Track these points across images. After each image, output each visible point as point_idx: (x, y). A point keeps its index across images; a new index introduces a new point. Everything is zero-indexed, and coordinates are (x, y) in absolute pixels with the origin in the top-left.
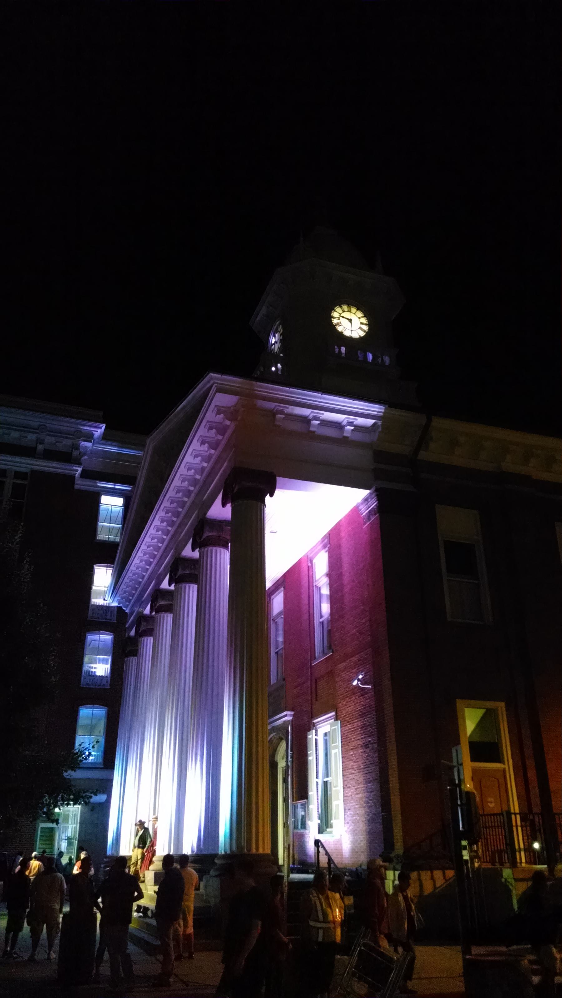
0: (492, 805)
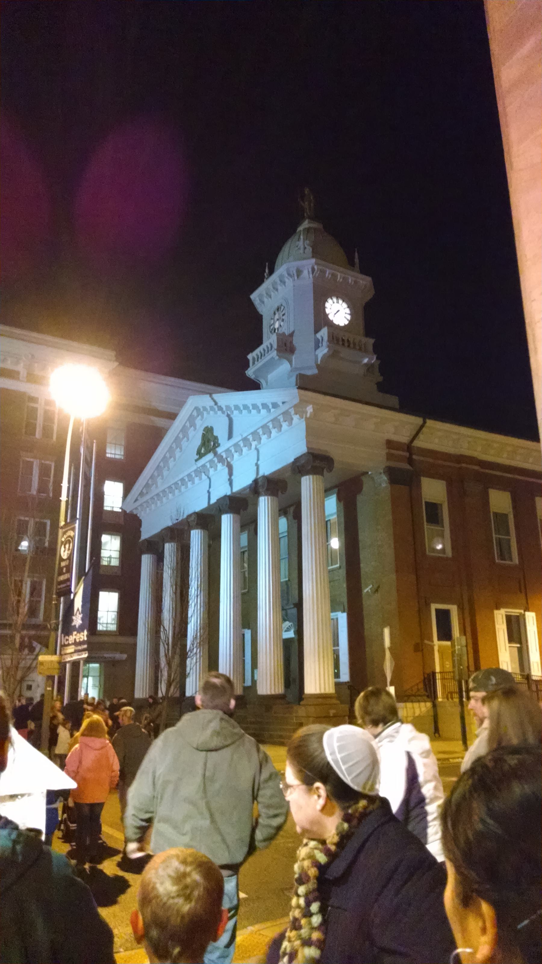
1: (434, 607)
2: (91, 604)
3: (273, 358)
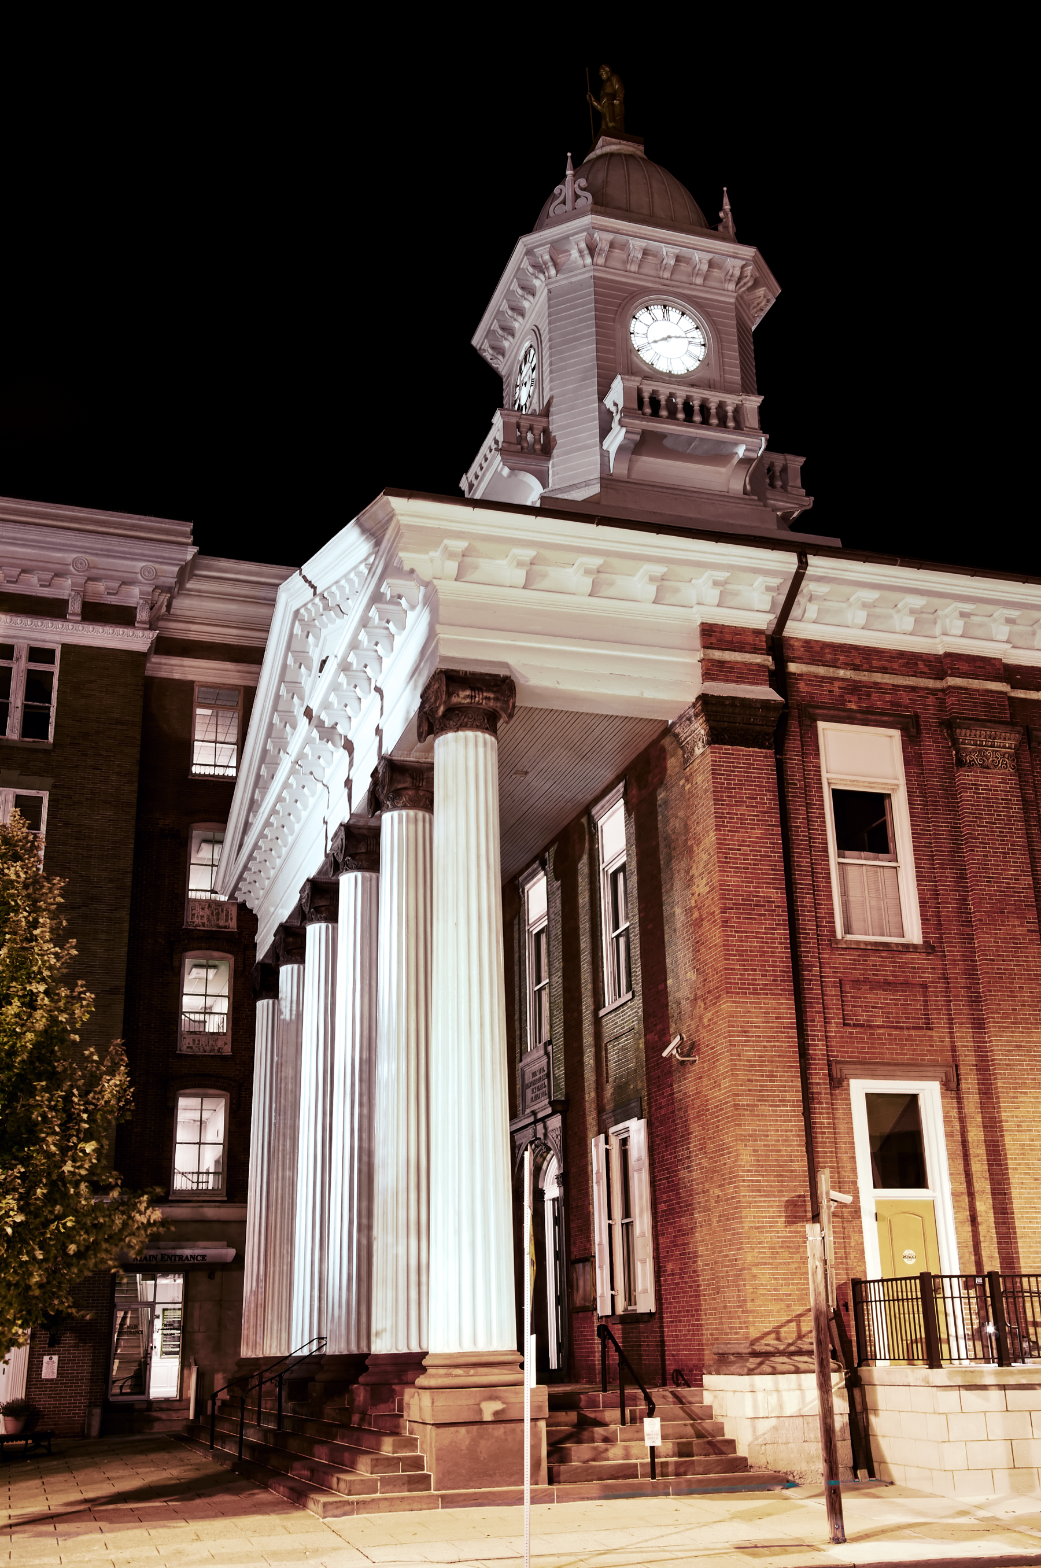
0: (910, 1262)
1: (859, 1089)
2: (975, 1255)
3: (497, 474)
